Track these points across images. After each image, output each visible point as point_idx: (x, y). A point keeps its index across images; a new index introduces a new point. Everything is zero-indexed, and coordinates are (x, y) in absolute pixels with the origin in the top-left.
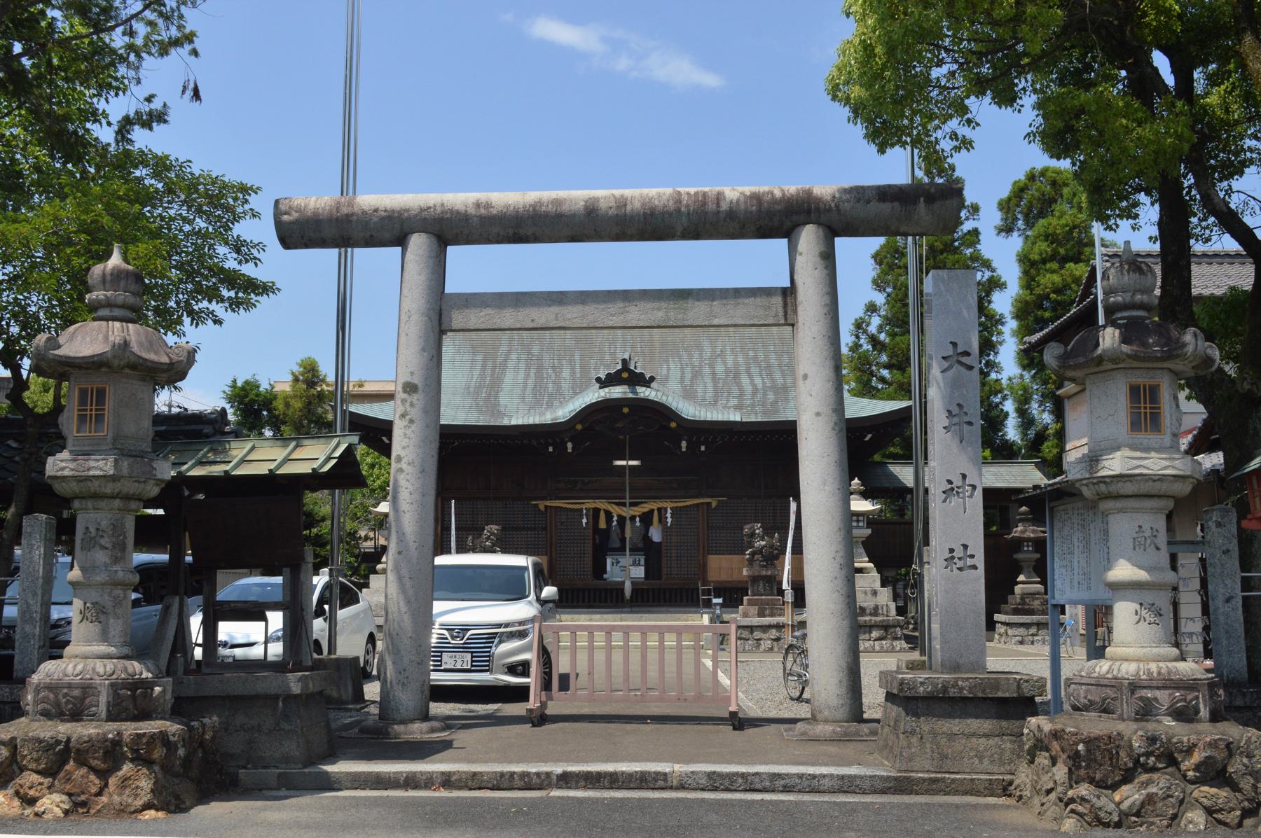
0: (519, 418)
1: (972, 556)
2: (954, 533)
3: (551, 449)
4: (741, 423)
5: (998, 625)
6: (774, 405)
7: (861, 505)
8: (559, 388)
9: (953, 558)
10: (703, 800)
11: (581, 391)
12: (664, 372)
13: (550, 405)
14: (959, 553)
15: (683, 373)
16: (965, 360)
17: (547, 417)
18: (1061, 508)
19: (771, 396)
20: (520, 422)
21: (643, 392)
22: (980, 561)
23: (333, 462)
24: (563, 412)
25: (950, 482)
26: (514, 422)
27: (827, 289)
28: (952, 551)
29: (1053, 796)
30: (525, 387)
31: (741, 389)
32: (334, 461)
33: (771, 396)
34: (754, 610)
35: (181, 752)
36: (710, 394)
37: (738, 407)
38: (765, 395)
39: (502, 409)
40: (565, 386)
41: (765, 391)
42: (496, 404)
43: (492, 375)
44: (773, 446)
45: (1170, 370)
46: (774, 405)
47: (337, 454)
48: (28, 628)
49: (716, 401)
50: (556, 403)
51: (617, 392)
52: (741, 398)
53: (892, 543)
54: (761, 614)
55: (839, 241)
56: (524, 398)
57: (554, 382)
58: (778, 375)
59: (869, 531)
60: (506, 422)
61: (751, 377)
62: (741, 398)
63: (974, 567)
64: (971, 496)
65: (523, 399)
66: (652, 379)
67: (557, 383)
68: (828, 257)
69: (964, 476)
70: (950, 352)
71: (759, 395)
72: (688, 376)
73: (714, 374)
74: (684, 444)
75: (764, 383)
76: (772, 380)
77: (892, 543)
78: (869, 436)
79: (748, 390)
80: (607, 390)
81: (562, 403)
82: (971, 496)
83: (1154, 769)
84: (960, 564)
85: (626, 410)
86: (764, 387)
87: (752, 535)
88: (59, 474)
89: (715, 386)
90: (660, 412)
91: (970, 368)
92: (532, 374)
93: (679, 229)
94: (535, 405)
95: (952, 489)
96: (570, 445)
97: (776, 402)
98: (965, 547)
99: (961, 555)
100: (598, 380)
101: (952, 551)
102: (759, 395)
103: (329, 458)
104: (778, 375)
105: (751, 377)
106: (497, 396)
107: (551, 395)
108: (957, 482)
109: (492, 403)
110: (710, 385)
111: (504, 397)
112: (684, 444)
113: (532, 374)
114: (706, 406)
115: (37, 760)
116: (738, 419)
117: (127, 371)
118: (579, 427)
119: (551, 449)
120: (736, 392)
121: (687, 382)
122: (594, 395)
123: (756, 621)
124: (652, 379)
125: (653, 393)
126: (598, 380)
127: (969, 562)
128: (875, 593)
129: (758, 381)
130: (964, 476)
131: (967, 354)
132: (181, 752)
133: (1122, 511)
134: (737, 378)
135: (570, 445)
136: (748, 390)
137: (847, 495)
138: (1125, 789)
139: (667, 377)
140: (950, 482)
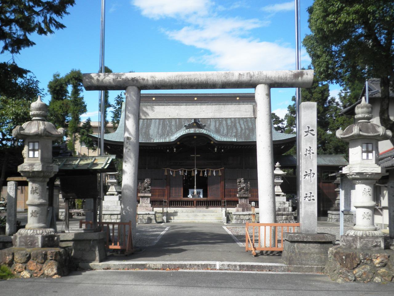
0: (157, 140)
1: (313, 196)
2: (308, 186)
3: (168, 151)
4: (236, 142)
5: (329, 215)
6: (249, 135)
7: (278, 172)
8: (171, 129)
9: (307, 197)
10: (226, 273)
11: (179, 130)
12: (209, 123)
13: (168, 135)
14: (309, 195)
15: (215, 123)
16: (312, 132)
17: (167, 140)
18: (345, 179)
19: (247, 132)
20: (157, 141)
21: (203, 131)
22: (316, 198)
23: (108, 165)
24: (174, 138)
25: (306, 172)
26: (155, 141)
27: (268, 106)
28: (306, 194)
29: (335, 272)
30: (159, 128)
31: (237, 129)
32: (108, 164)
33: (247, 132)
34: (241, 209)
35: (64, 257)
36: (225, 131)
37: (236, 136)
38: (245, 132)
39: (151, 136)
40: (173, 128)
41: (245, 130)
42: (149, 135)
43: (147, 124)
44: (248, 150)
45: (376, 139)
46: (249, 135)
47: (109, 162)
48: (10, 218)
49: (228, 134)
50: (170, 134)
51: (192, 131)
52: (236, 133)
53: (290, 186)
54: (243, 211)
55: (272, 89)
56: (158, 132)
57: (169, 127)
58: (250, 124)
59: (282, 181)
60: (152, 141)
61: (240, 125)
62: (236, 133)
63: (314, 200)
64: (313, 177)
65: (158, 132)
66: (205, 126)
67: (170, 127)
68: (269, 95)
69: (311, 170)
70: (307, 130)
71: (243, 131)
72: (217, 124)
73: (227, 123)
74: (216, 149)
75: (245, 127)
76: (248, 126)
77: (290, 186)
78: (283, 147)
79: (239, 129)
80: (188, 130)
81: (173, 134)
82: (313, 177)
83: (366, 264)
84: (309, 199)
85: (195, 137)
86: (245, 129)
87: (240, 182)
88: (24, 170)
89: (227, 129)
90: (206, 138)
91: (314, 135)
92: (161, 123)
93: (218, 87)
94: (162, 135)
95: (307, 174)
96: (175, 149)
97: (249, 134)
98: (311, 193)
99: (310, 196)
100: (185, 126)
101: (306, 194)
102: (243, 131)
103: (106, 164)
104: (250, 124)
105: (240, 125)
106: (149, 131)
107: (168, 131)
108: (309, 172)
109: (147, 134)
110: (225, 128)
111: (151, 132)
112: (216, 149)
113: (161, 123)
114: (224, 136)
115: (21, 260)
116: (236, 140)
117: (45, 137)
118: (178, 143)
119: (168, 151)
120: (235, 131)
121: (217, 126)
122: (183, 132)
123: (241, 213)
124: (205, 126)
125: (205, 131)
126: (185, 126)
127: (312, 198)
128: (284, 203)
129: (243, 126)
130: (311, 170)
131: (312, 130)
132: (64, 257)
133: (359, 183)
134: (235, 125)
135: (175, 149)
136: (239, 129)
137: (274, 168)
138: (357, 270)
139: (210, 125)
140: (306, 172)
